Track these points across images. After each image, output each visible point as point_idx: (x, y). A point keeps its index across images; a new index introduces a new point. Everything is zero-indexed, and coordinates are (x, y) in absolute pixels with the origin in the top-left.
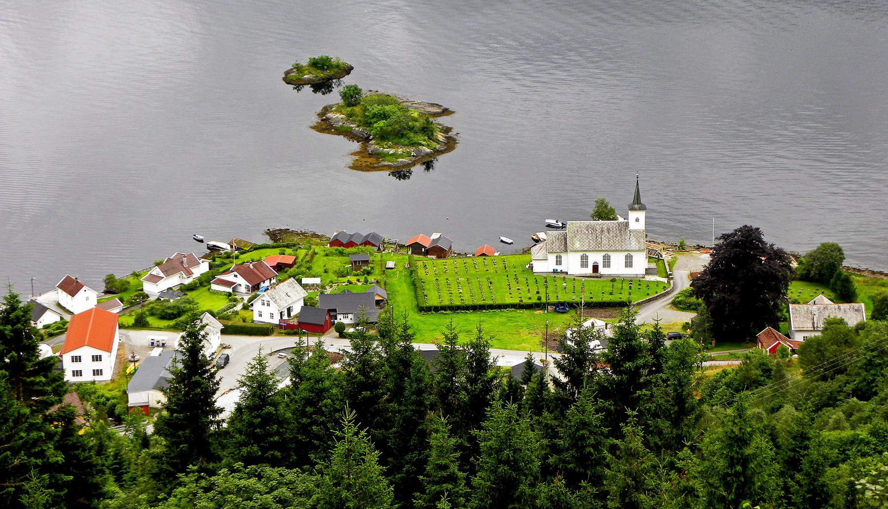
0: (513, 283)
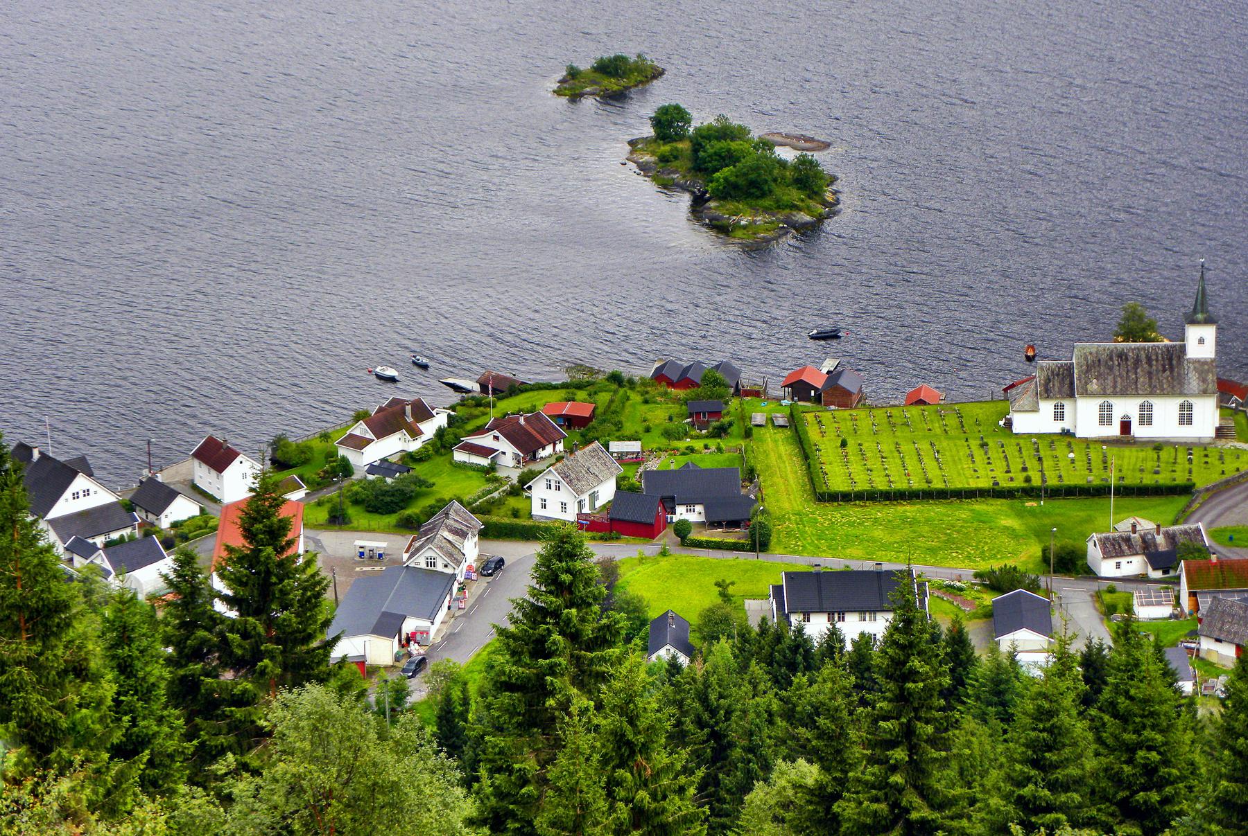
0: (979, 454)
